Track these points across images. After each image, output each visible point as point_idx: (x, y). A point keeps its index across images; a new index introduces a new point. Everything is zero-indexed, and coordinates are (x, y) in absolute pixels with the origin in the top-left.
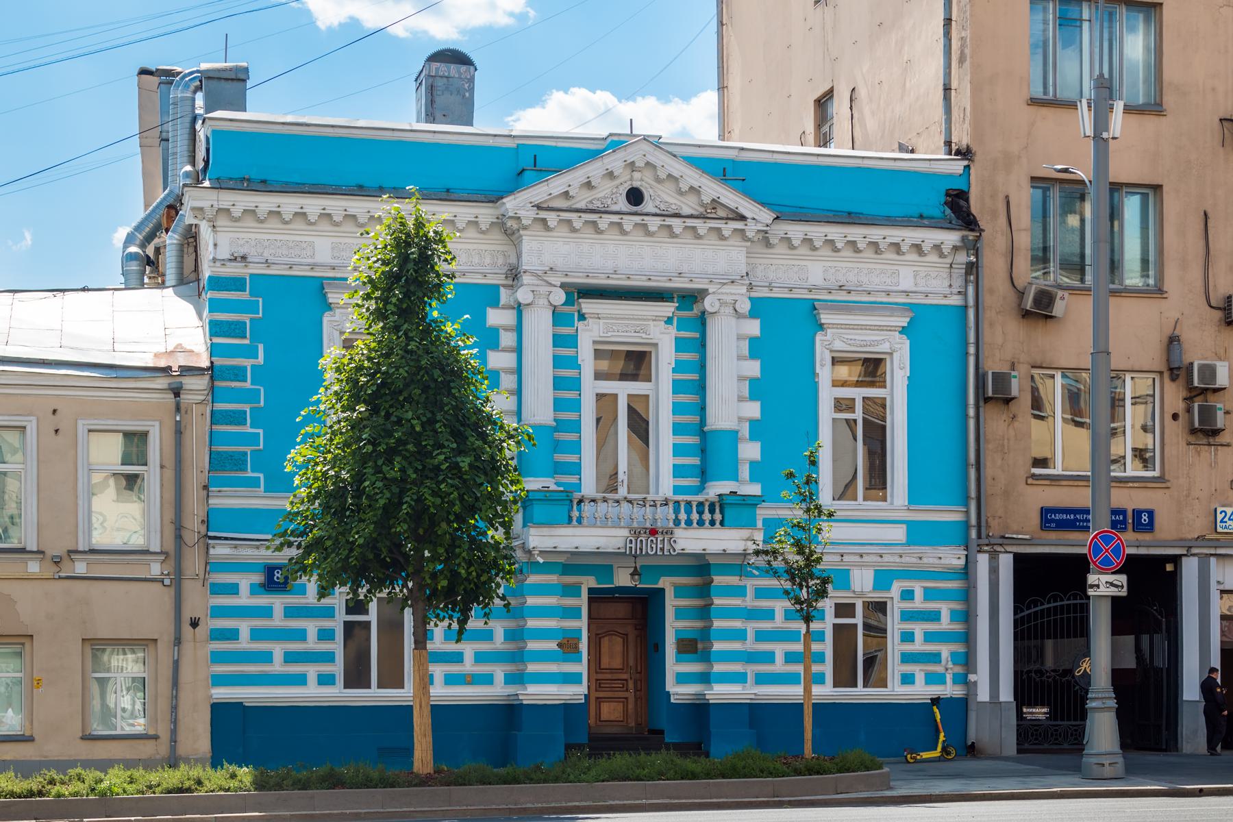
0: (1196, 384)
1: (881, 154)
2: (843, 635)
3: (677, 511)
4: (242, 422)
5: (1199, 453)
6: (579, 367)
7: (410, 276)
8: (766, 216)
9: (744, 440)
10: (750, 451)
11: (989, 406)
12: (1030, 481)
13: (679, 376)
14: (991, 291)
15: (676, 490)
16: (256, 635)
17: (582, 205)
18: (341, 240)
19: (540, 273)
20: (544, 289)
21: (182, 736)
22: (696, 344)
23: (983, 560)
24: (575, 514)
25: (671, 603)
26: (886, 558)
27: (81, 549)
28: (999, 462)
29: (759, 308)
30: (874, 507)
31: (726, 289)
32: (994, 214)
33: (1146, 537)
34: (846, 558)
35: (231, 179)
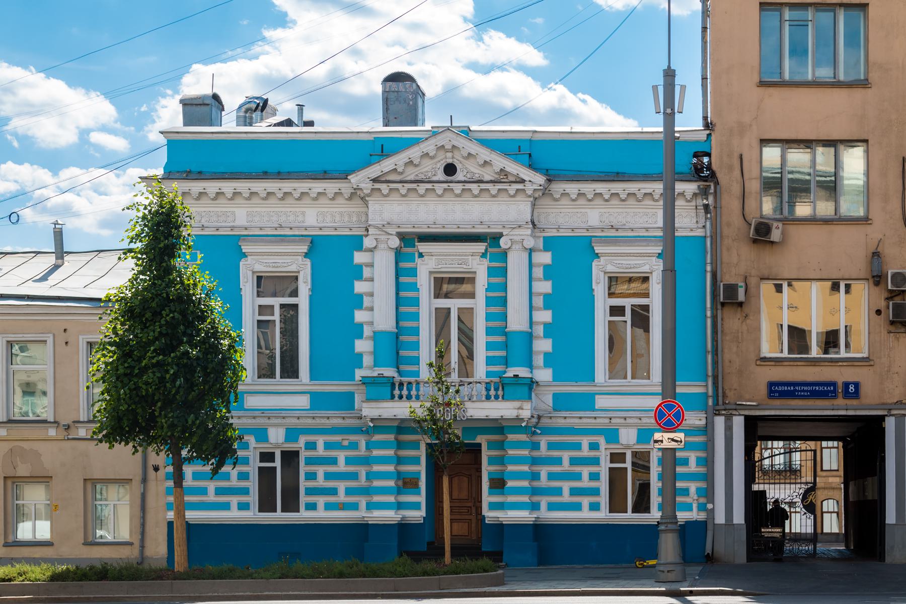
0: (890, 288)
2: (266, 476)
3: (488, 390)
5: (898, 339)
6: (418, 290)
7: (642, 355)
8: (540, 179)
9: (538, 337)
10: (543, 345)
11: (726, 309)
12: (758, 363)
13: (490, 294)
14: (729, 225)
15: (488, 374)
16: (328, 476)
17: (411, 178)
18: (255, 209)
19: (380, 226)
20: (383, 237)
21: (148, 543)
22: (500, 272)
23: (720, 422)
24: (414, 392)
25: (485, 454)
26: (644, 420)
27: (82, 420)
28: (735, 349)
29: (549, 244)
30: (289, 384)
31: (517, 232)
32: (731, 168)
33: (854, 402)
34: (613, 421)
35: (178, 172)
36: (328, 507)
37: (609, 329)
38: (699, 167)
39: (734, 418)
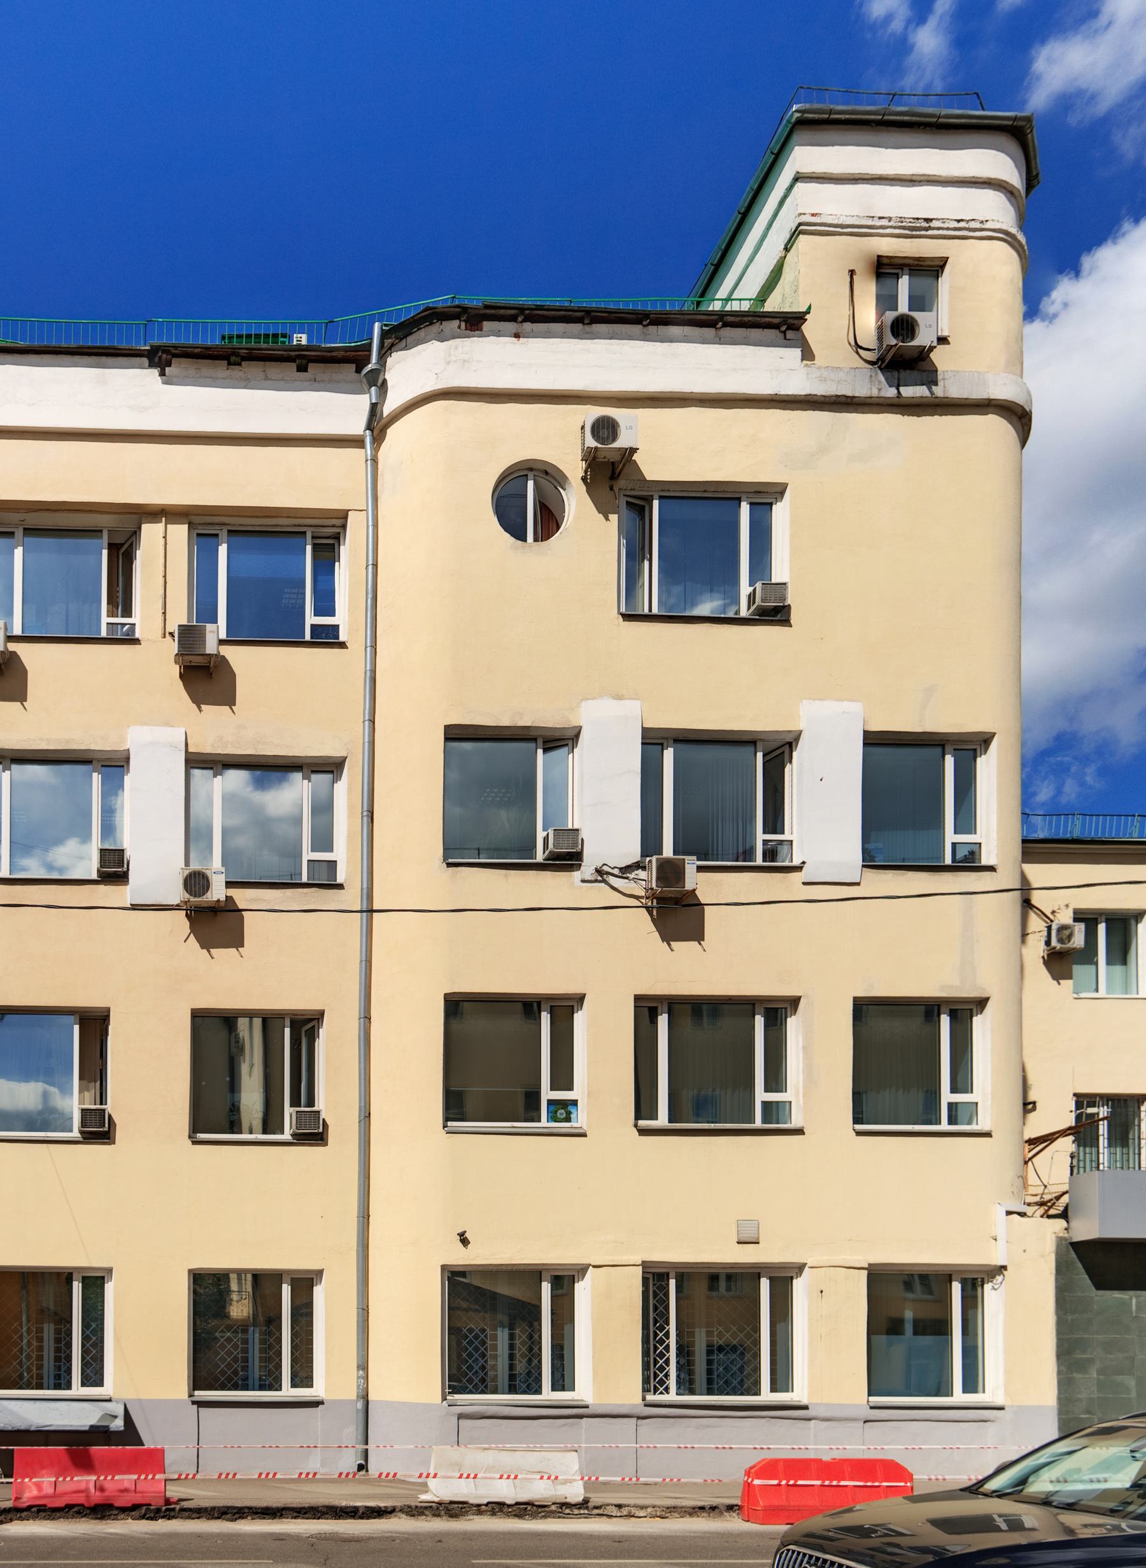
1: (770, 310)
4: (954, 1090)
7: (605, 429)
36: (546, 840)
37: (552, 1314)
38: (1079, 1355)
39: (939, 87)
